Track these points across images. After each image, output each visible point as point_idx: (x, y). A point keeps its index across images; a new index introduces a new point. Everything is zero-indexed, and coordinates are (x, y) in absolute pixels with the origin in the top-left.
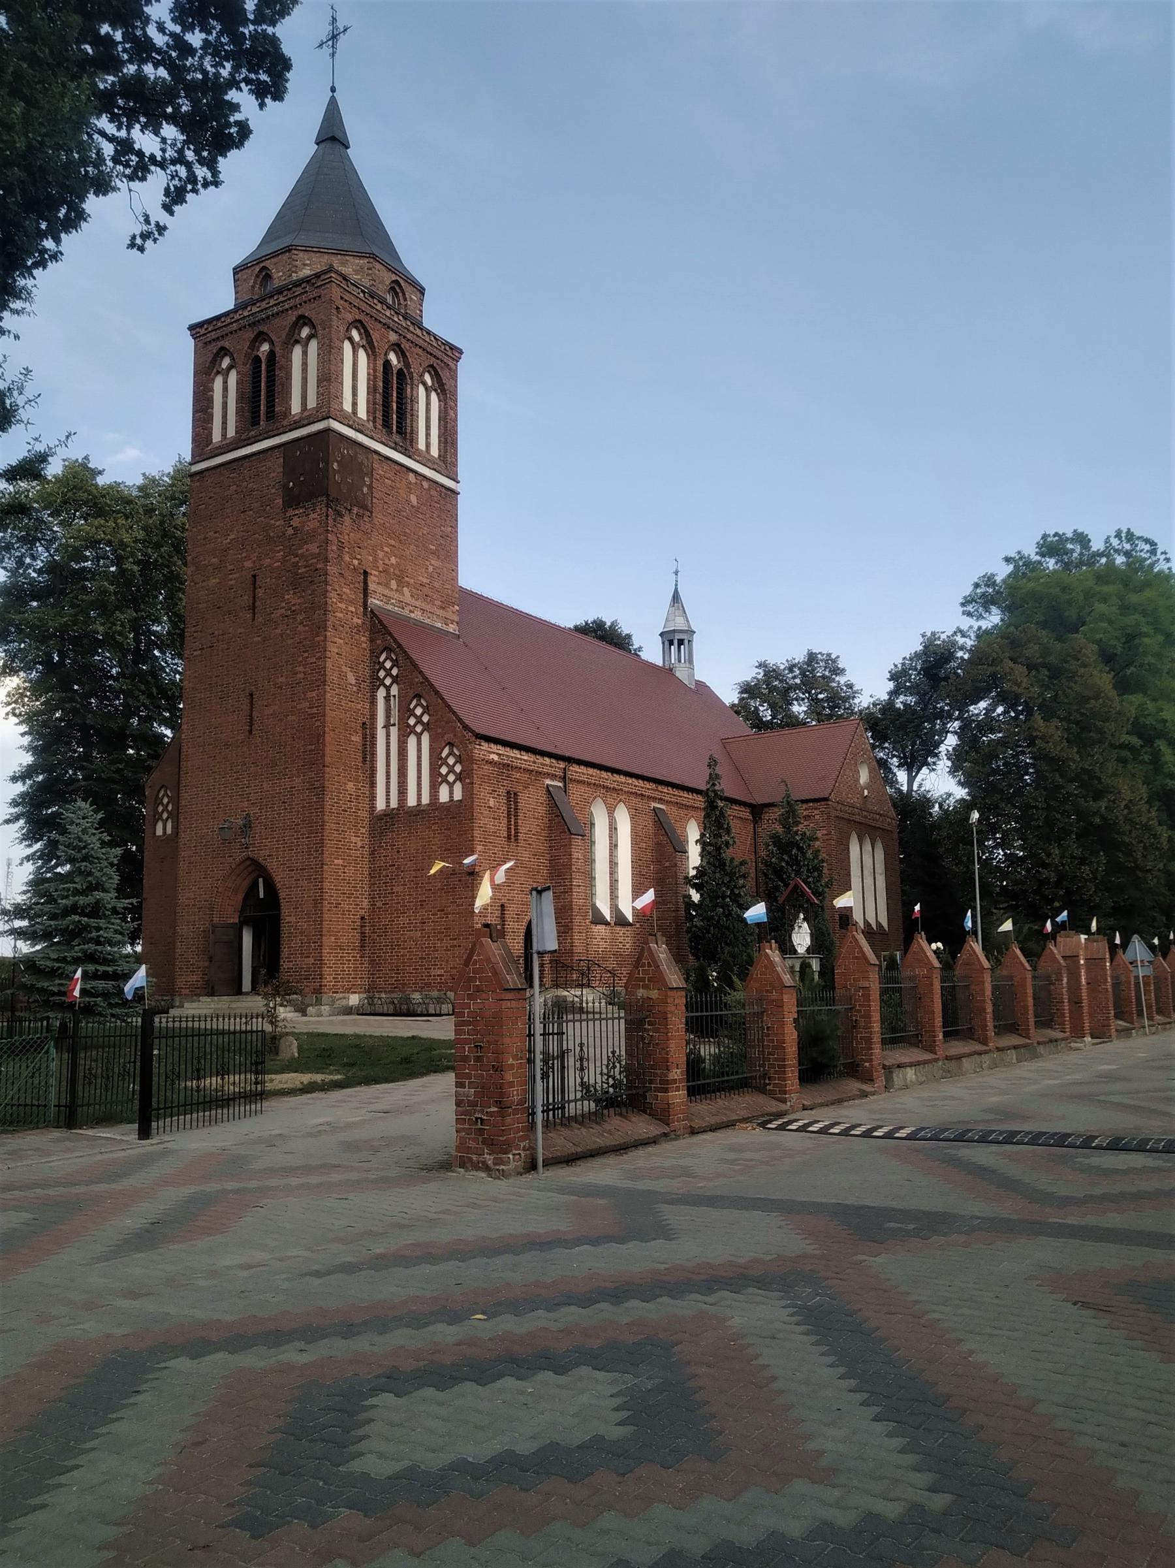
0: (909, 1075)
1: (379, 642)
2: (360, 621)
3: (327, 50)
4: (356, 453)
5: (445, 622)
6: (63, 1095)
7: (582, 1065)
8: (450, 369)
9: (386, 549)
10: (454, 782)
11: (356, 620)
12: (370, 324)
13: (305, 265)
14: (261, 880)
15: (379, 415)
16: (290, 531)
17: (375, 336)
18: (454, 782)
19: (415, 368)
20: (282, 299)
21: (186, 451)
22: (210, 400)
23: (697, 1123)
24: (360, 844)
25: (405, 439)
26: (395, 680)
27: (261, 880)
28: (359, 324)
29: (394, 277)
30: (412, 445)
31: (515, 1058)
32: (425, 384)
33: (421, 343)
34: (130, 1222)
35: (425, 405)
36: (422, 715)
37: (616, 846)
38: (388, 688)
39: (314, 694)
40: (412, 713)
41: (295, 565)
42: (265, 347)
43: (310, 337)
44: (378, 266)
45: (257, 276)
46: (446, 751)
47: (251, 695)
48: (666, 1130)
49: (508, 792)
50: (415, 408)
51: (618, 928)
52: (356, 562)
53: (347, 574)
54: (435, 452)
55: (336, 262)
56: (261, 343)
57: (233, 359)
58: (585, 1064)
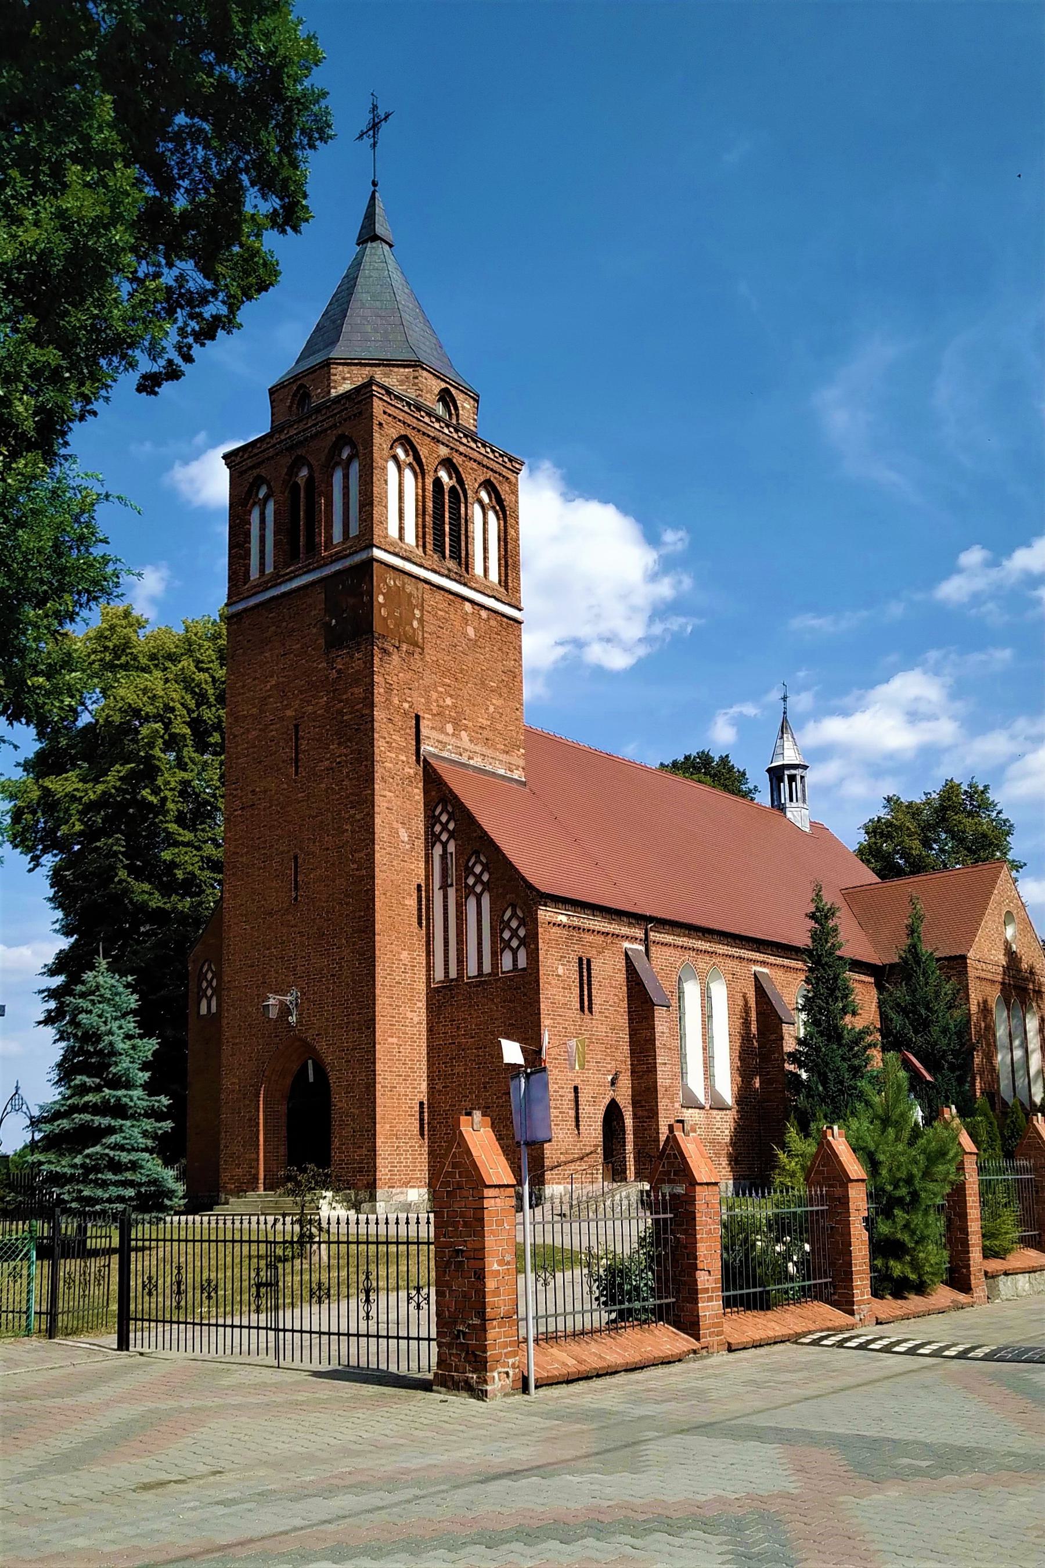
0: (1020, 1284)
1: (434, 793)
2: (412, 771)
3: (368, 141)
4: (404, 584)
5: (509, 766)
6: (44, 1304)
7: (179, 1287)
8: (510, 483)
9: (440, 689)
10: (518, 947)
11: (407, 770)
12: (416, 439)
13: (344, 379)
14: (310, 1062)
15: (429, 539)
16: (334, 674)
17: (423, 452)
18: (518, 947)
19: (471, 484)
20: (320, 418)
21: (220, 593)
22: (248, 534)
23: (735, 1339)
24: (416, 1020)
25: (460, 564)
26: (452, 835)
27: (310, 1062)
28: (404, 441)
29: (443, 385)
30: (467, 571)
31: (501, 1262)
32: (480, 502)
33: (475, 455)
34: (62, 1443)
35: (482, 527)
36: (482, 873)
37: (710, 1017)
38: (444, 845)
39: (362, 855)
40: (469, 871)
41: (340, 712)
42: (304, 472)
43: (350, 459)
44: (425, 374)
45: (294, 395)
46: (508, 914)
47: (296, 858)
48: (696, 1345)
49: (580, 959)
50: (470, 528)
51: (715, 1112)
52: (406, 705)
53: (397, 718)
54: (494, 576)
55: (379, 375)
56: (299, 469)
57: (269, 487)
58: (175, 1287)
